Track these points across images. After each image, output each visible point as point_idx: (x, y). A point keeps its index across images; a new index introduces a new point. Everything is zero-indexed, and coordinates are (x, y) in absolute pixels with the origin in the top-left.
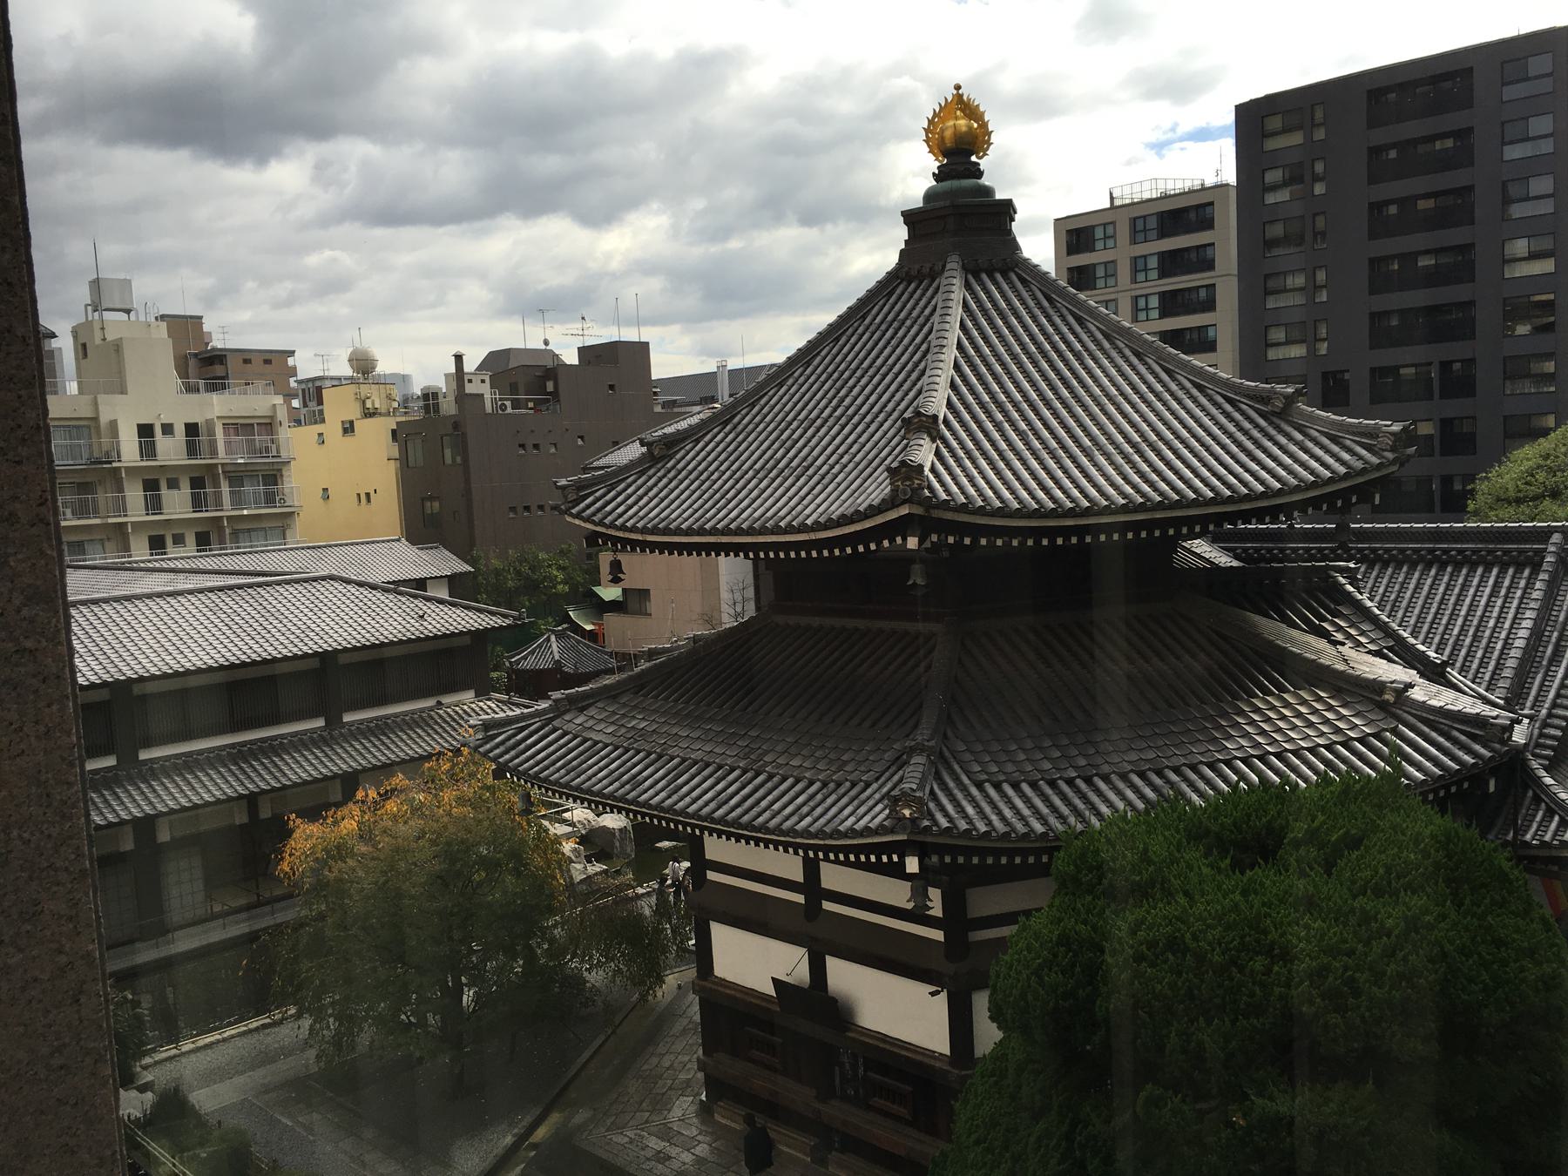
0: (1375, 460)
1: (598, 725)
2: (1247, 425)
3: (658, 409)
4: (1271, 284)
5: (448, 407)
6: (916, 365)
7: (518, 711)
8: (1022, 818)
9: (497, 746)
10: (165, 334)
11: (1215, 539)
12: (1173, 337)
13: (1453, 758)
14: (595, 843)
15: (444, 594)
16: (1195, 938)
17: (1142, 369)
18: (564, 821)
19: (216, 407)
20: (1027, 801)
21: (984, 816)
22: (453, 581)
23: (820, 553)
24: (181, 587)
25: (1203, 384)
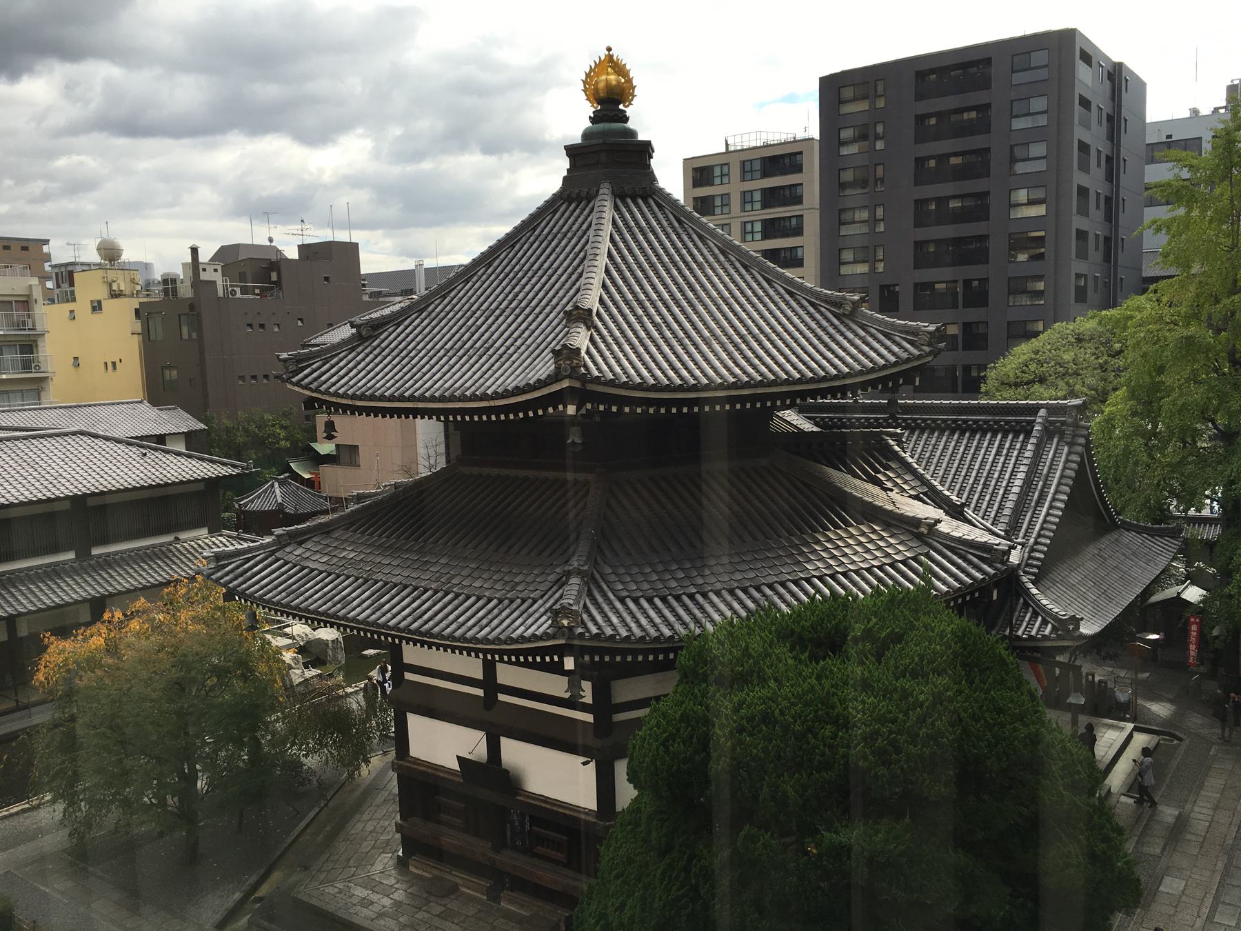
0: (916, 352)
1: (313, 555)
3: (366, 298)
4: (847, 216)
5: (186, 291)
7: (245, 545)
8: (655, 625)
11: (801, 410)
12: (771, 254)
13: (968, 575)
15: (182, 448)
17: (748, 278)
20: (659, 612)
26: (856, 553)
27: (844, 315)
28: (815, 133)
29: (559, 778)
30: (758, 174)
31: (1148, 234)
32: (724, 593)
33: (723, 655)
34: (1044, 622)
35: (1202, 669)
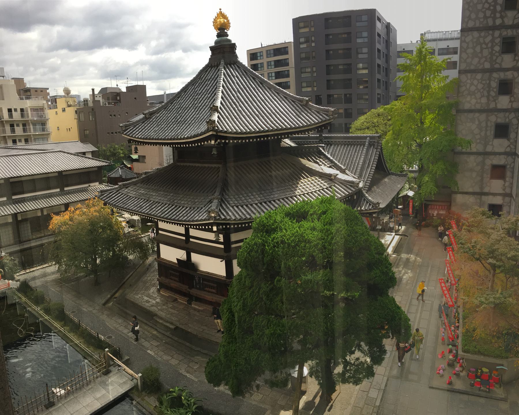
0: (328, 118)
1: (131, 192)
2: (298, 108)
3: (148, 105)
4: (303, 70)
5: (91, 104)
6: (213, 92)
7: (110, 188)
8: (244, 215)
9: (104, 197)
10: (14, 83)
11: (291, 139)
12: (279, 84)
13: (347, 191)
14: (131, 223)
15: (90, 156)
16: (287, 240)
17: (270, 92)
18: (123, 217)
19: (28, 104)
20: (245, 210)
21: (234, 215)
22: (93, 152)
23: (189, 145)
24: (21, 153)
25: (286, 97)
26: (311, 187)
27: (304, 105)
28: (291, 40)
29: (212, 266)
30: (272, 55)
31: (398, 81)
32: (268, 202)
33: (268, 223)
34: (370, 205)
35: (413, 215)
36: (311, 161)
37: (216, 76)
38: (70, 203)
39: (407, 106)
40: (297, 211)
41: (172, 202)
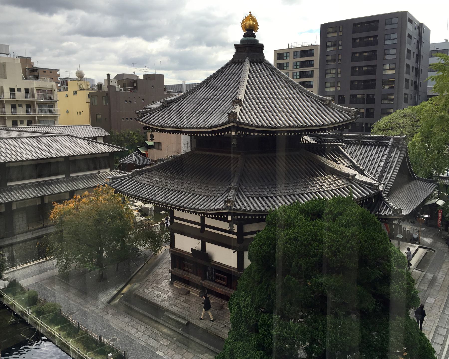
0: (350, 118)
1: (145, 179)
3: (166, 93)
5: (105, 89)
6: (236, 86)
7: (122, 175)
8: (259, 207)
9: (116, 184)
12: (303, 83)
13: (365, 193)
16: (301, 237)
17: (294, 91)
18: (135, 206)
19: (34, 84)
20: (260, 202)
22: (105, 138)
24: (22, 136)
25: (309, 96)
26: (327, 185)
28: (318, 43)
30: (299, 56)
32: (283, 196)
33: (282, 217)
34: (390, 210)
36: (328, 159)
37: (240, 72)
38: (76, 190)
39: (440, 107)
40: (312, 209)
41: (188, 190)
